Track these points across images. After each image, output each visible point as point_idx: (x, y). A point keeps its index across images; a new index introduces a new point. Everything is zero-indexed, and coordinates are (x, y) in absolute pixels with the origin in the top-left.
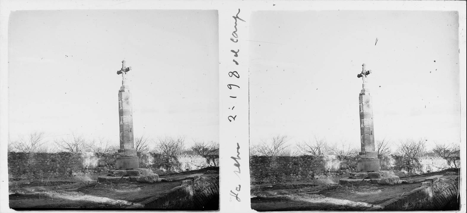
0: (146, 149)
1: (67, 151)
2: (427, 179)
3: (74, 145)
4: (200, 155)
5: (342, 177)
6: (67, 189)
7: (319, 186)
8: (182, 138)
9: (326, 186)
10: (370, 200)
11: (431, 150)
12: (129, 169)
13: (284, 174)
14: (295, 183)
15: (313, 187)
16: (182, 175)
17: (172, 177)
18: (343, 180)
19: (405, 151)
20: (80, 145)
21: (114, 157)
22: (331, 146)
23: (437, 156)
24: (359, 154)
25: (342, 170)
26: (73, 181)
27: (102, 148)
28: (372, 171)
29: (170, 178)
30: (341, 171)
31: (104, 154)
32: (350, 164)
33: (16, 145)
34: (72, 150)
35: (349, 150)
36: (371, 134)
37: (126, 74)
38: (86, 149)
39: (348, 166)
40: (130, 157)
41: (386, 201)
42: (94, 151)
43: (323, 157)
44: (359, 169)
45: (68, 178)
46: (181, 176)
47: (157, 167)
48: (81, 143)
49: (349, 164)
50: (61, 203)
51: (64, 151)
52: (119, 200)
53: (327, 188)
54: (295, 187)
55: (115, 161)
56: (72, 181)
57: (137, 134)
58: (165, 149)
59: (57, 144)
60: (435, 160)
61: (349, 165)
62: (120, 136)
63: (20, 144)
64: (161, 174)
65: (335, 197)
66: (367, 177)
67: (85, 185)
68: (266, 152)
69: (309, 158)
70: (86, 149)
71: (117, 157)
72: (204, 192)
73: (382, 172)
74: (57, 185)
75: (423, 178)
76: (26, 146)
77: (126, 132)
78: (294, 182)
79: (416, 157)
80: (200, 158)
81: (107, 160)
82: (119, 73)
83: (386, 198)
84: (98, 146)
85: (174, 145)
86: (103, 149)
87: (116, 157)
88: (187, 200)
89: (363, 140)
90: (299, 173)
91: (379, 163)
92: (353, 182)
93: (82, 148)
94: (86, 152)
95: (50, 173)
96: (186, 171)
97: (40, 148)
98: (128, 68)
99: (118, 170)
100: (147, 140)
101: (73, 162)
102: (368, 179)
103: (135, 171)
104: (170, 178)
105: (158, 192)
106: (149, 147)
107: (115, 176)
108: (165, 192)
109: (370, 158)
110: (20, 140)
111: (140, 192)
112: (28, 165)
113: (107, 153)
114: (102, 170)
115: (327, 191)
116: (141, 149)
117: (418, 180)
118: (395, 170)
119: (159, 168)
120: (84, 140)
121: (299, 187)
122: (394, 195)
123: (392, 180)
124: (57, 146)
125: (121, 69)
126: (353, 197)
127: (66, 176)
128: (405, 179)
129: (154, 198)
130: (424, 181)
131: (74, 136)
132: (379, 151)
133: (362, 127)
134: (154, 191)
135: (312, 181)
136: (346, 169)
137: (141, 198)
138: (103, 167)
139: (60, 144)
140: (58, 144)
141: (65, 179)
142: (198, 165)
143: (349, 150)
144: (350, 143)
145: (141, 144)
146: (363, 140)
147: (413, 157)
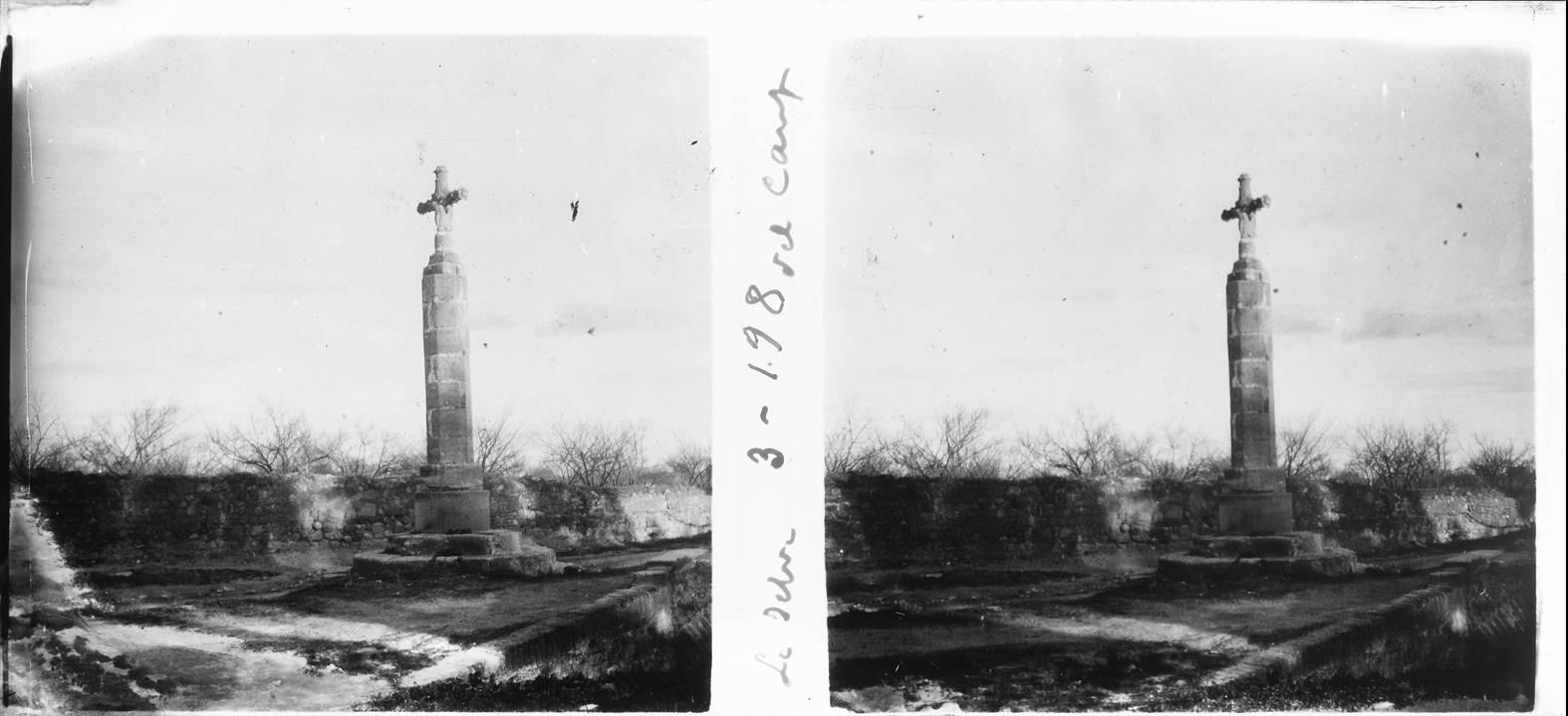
0: (516, 466)
1: (252, 470)
2: (1448, 560)
3: (275, 452)
4: (699, 486)
5: (359, 548)
6: (1059, 595)
7: (1090, 579)
8: (1438, 432)
9: (307, 576)
10: (1259, 626)
11: (663, 463)
12: (456, 532)
13: (168, 534)
14: (204, 565)
15: (1073, 579)
16: (635, 552)
17: (602, 561)
18: (364, 557)
19: (1376, 468)
20: (296, 450)
21: (409, 490)
22: (1132, 447)
23: (1486, 487)
24: (1222, 475)
25: (360, 523)
26: (1081, 571)
27: (1178, 466)
28: (464, 532)
29: (595, 562)
30: (357, 528)
31: (373, 481)
32: (389, 505)
33: (87, 449)
34: (269, 466)
35: (1193, 463)
36: (460, 405)
37: (447, 212)
38: (314, 464)
39: (381, 512)
40: (1263, 494)
41: (513, 631)
42: (339, 470)
43: (1106, 483)
44: (419, 523)
45: (257, 559)
46: (633, 556)
47: (551, 527)
48: (299, 445)
49: (386, 507)
50: (1035, 640)
51: (243, 468)
52: (1224, 632)
53: (1118, 583)
54: (206, 577)
55: (411, 505)
56: (268, 569)
57: (482, 413)
58: (1382, 469)
59: (217, 447)
60: (1478, 498)
61: (383, 508)
62: (427, 421)
63: (98, 445)
64: (563, 549)
65: (1140, 615)
66: (448, 550)
67: (311, 582)
68: (111, 460)
69: (1061, 487)
70: (314, 464)
71: (418, 491)
72: (1501, 609)
73: (498, 535)
74: (218, 582)
75: (1437, 557)
76: (119, 454)
77: (448, 408)
78: (203, 562)
79: (1413, 489)
80: (696, 498)
81: (384, 500)
82: (424, 208)
83: (512, 620)
84: (355, 454)
85: (610, 452)
86: (370, 464)
87: (414, 490)
88: (651, 637)
89: (435, 425)
90: (220, 531)
91: (1291, 507)
92: (1204, 567)
93: (300, 461)
94: (316, 475)
95: (196, 543)
96: (1450, 540)
97: (162, 460)
98: (456, 193)
99: (419, 532)
100: (518, 434)
101: (273, 506)
102: (450, 555)
103: (1281, 541)
104: (1396, 563)
105: (552, 609)
106: (1330, 460)
107: (410, 555)
108: (575, 608)
109: (456, 486)
110: (912, 439)
111: (494, 610)
112: (124, 516)
113: (383, 477)
114: (1174, 537)
115: (1115, 598)
116: (496, 467)
117: (1421, 563)
118: (540, 529)
119: (558, 529)
120: (307, 435)
121: (218, 577)
122: (541, 614)
123: (533, 561)
124: (220, 454)
125: (433, 196)
126: (401, 615)
127: (248, 552)
128: (1375, 562)
129: (540, 627)
130: (1441, 568)
131: (274, 419)
132: (484, 462)
133: (430, 381)
134: (540, 606)
135: (1071, 560)
136: (375, 522)
137: (497, 627)
138: (369, 525)
139: (230, 445)
140: (222, 447)
141: (245, 563)
142: (1490, 520)
143: (384, 460)
144: (387, 436)
145: (496, 448)
146: (433, 426)
147: (1405, 487)
